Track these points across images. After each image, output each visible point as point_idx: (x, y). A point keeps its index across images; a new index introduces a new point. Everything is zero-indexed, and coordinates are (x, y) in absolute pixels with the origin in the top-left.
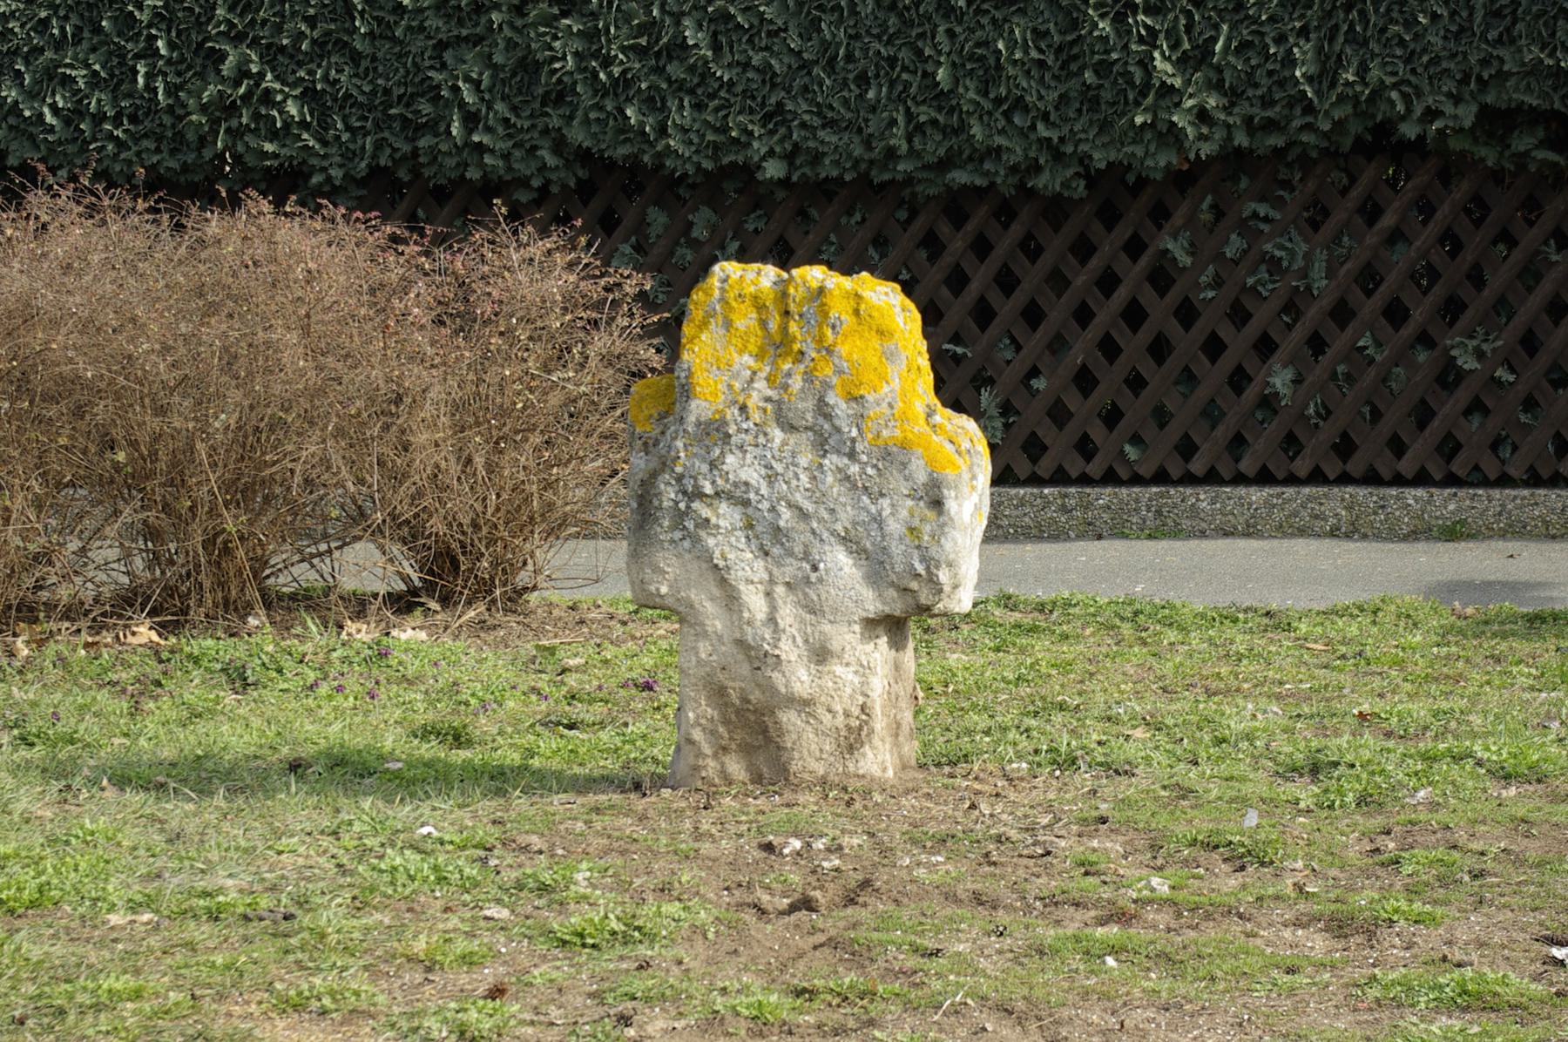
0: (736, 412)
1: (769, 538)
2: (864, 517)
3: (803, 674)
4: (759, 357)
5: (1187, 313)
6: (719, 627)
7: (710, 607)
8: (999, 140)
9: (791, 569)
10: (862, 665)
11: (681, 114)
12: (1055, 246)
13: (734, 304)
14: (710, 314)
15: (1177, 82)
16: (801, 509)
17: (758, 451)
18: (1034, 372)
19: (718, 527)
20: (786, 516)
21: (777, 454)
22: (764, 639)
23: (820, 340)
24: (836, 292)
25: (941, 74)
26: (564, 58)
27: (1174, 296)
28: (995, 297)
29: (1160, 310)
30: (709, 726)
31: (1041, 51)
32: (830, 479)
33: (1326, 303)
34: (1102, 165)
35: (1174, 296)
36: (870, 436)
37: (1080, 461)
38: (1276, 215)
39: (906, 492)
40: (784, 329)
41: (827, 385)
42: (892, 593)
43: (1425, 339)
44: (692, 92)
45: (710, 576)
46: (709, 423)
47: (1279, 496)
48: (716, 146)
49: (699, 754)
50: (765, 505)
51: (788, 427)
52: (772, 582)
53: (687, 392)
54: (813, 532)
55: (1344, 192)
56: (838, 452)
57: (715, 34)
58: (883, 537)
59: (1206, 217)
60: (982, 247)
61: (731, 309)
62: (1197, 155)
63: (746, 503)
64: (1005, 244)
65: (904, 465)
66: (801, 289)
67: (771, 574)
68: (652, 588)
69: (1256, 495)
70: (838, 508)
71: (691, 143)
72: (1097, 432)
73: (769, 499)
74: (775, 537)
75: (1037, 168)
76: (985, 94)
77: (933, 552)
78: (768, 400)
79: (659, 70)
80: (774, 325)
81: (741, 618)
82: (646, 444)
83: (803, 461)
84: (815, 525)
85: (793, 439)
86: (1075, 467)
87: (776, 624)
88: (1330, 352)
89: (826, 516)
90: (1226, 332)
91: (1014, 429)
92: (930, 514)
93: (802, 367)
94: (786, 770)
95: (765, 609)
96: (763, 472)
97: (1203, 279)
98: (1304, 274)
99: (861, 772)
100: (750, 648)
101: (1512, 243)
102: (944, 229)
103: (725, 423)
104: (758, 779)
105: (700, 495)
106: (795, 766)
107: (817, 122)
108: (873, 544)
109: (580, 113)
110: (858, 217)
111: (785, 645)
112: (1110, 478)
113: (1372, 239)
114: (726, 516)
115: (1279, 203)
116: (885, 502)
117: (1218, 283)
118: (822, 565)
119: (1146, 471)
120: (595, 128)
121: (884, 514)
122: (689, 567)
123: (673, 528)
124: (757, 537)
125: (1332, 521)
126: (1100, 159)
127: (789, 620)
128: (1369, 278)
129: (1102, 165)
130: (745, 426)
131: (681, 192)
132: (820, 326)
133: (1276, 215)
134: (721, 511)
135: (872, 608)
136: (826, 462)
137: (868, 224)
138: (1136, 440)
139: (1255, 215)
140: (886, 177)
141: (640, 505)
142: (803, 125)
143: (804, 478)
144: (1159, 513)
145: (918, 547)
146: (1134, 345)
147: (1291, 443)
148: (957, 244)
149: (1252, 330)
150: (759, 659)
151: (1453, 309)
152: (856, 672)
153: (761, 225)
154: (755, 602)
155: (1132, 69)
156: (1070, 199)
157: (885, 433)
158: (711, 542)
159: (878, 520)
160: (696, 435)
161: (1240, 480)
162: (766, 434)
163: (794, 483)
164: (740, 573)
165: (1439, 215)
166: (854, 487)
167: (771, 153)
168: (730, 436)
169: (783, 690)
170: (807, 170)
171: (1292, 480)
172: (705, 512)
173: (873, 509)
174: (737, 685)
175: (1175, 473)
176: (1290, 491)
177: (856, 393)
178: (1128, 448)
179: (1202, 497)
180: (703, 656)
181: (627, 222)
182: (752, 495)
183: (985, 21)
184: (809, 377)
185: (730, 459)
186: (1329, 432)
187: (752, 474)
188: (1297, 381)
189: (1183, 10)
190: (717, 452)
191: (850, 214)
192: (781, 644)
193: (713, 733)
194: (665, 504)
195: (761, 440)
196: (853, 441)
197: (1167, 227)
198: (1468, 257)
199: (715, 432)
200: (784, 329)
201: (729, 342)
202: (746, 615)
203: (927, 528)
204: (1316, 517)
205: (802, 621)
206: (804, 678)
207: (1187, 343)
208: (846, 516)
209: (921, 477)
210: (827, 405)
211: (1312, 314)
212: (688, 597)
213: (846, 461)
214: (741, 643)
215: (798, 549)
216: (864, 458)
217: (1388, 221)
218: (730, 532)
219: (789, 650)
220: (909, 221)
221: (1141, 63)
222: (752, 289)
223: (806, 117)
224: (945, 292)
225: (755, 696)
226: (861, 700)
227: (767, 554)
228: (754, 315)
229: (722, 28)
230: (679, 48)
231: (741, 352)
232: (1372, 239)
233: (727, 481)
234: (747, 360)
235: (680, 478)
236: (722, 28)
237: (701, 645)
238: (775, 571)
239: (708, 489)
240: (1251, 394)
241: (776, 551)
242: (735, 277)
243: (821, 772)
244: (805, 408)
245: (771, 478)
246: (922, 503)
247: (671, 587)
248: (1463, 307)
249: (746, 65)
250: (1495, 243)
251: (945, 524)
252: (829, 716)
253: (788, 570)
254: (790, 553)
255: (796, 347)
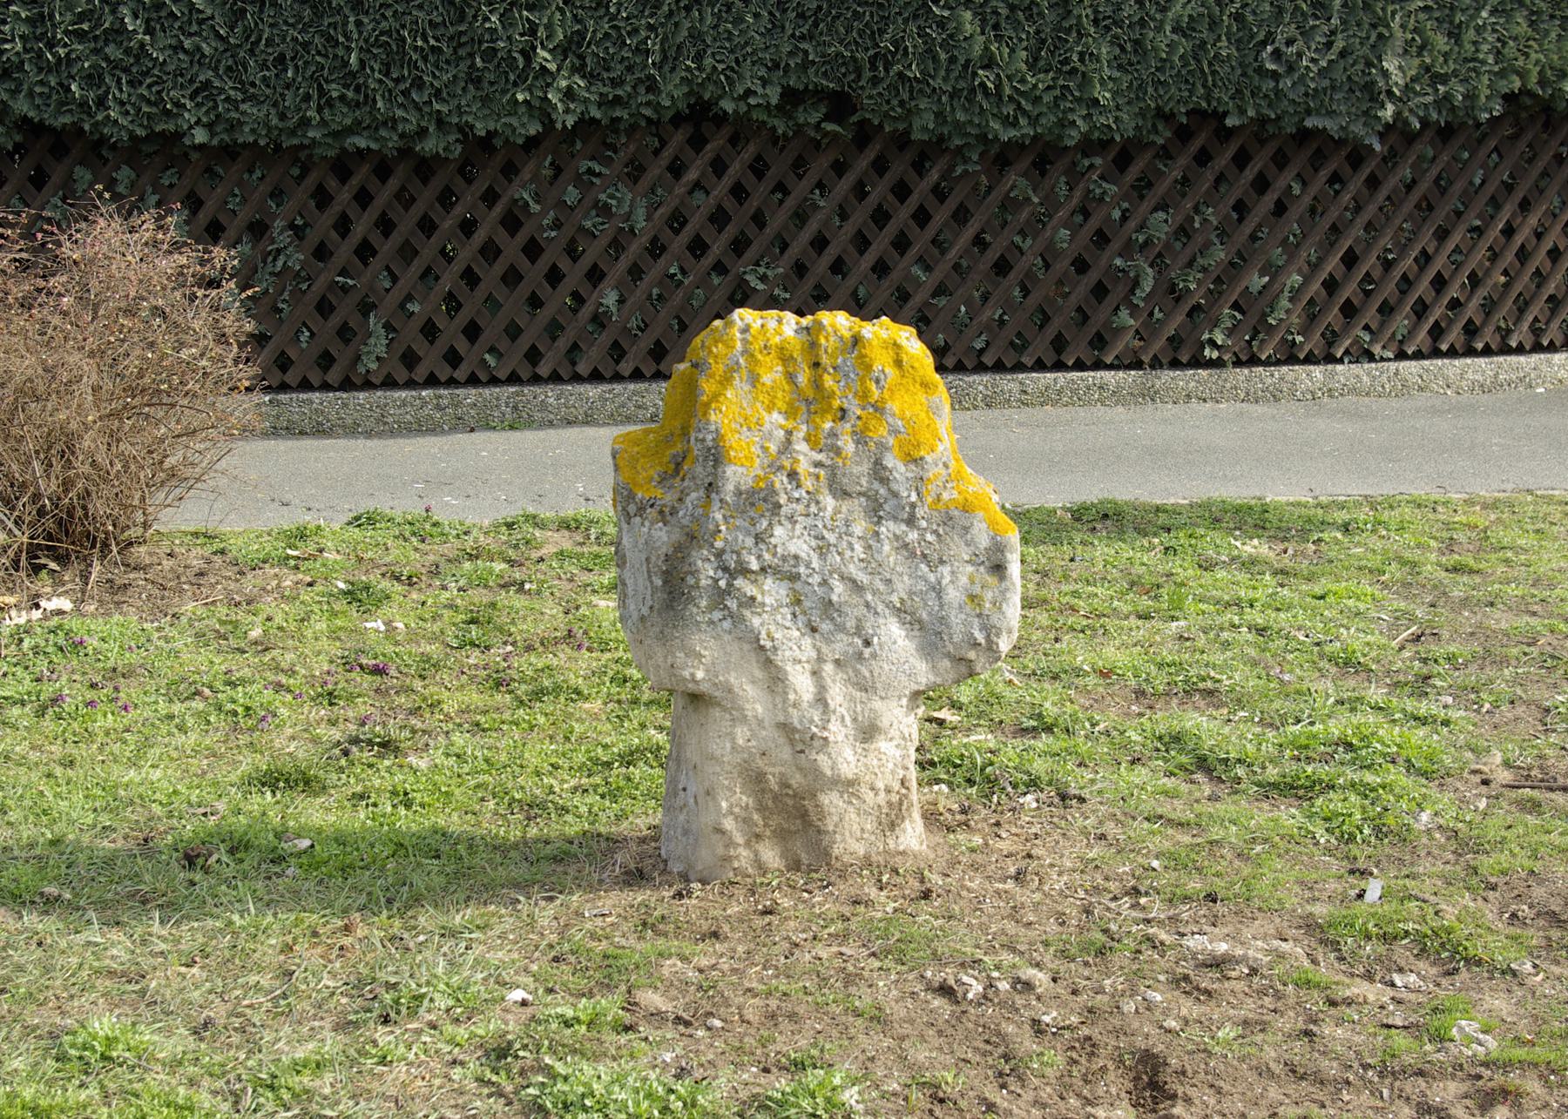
0: (785, 480)
1: (818, 614)
2: (921, 586)
3: (848, 753)
4: (790, 413)
5: (533, 250)
6: (760, 710)
7: (750, 691)
8: (399, 113)
9: (842, 645)
10: (904, 738)
11: (119, 91)
12: (426, 197)
13: (759, 357)
14: (733, 368)
15: (552, 67)
16: (854, 581)
17: (810, 521)
18: (409, 298)
19: (763, 604)
20: (839, 590)
21: (829, 523)
22: (812, 721)
23: (864, 395)
24: (875, 343)
25: (353, 59)
26: (13, 40)
27: (522, 237)
28: (375, 239)
29: (512, 249)
30: (743, 814)
31: (437, 40)
32: (887, 548)
33: (644, 240)
34: (483, 133)
35: (522, 237)
36: (930, 500)
37: (448, 369)
38: (605, 171)
39: (967, 558)
40: (817, 384)
41: (882, 447)
42: (946, 663)
43: (720, 268)
44: (126, 70)
45: (753, 657)
46: (752, 492)
47: (610, 392)
48: (149, 116)
49: (730, 843)
50: (816, 579)
51: (842, 494)
52: (820, 659)
53: (716, 456)
54: (867, 605)
55: (656, 152)
56: (895, 519)
57: (148, 21)
58: (941, 606)
59: (547, 172)
60: (363, 198)
61: (757, 362)
62: (564, 126)
63: (794, 578)
64: (384, 196)
65: (966, 529)
66: (832, 339)
67: (819, 651)
68: (686, 674)
69: (592, 391)
70: (895, 578)
71: (127, 113)
72: (462, 346)
73: (821, 573)
74: (825, 612)
75: (422, 133)
76: (387, 74)
77: (994, 620)
78: (818, 464)
79: (96, 51)
80: (803, 378)
81: (785, 701)
82: (661, 512)
83: (859, 528)
84: (869, 597)
85: (845, 506)
86: (444, 373)
87: (826, 705)
88: (647, 279)
89: (882, 587)
90: (564, 264)
91: (395, 345)
92: (991, 580)
93: (848, 426)
94: (828, 854)
95: (812, 689)
96: (814, 543)
97: (546, 222)
98: (628, 217)
99: (901, 848)
100: (794, 730)
101: (786, 193)
102: (332, 184)
103: (774, 492)
104: (795, 866)
105: (744, 571)
106: (836, 850)
107: (240, 96)
108: (930, 614)
109: (25, 87)
110: (258, 173)
111: (834, 726)
112: (473, 381)
113: (680, 190)
114: (772, 592)
115: (607, 162)
116: (945, 570)
117: (557, 225)
118: (875, 639)
119: (502, 375)
120: (38, 101)
121: (944, 582)
122: (728, 649)
123: (711, 608)
124: (804, 613)
125: (652, 410)
126: (480, 129)
127: (839, 699)
128: (677, 221)
129: (483, 133)
130: (797, 495)
131: (104, 153)
132: (863, 383)
133: (605, 171)
134: (766, 588)
135: (924, 681)
136: (883, 529)
137: (268, 179)
138: (492, 350)
139: (590, 171)
140: (295, 141)
141: (665, 582)
142: (228, 99)
143: (858, 548)
144: (515, 408)
145: (979, 616)
146: (491, 276)
147: (617, 352)
148: (344, 197)
149: (585, 263)
150: (801, 741)
151: (739, 246)
152: (897, 746)
153: (174, 180)
154: (801, 683)
155: (515, 55)
156: (447, 159)
157: (945, 496)
158: (756, 621)
159: (938, 590)
160: (736, 505)
161: (577, 378)
162: (818, 503)
163: (848, 553)
164: (787, 653)
165: (731, 171)
166: (913, 554)
167: (198, 122)
168: (780, 506)
169: (829, 773)
170: (226, 137)
171: (618, 378)
172: (750, 589)
173: (932, 578)
174: (777, 770)
175: (525, 375)
176: (618, 387)
177: (916, 455)
178: (487, 356)
179: (549, 394)
180: (741, 742)
181: (56, 178)
182: (802, 570)
183: (389, 13)
184: (860, 438)
185: (779, 531)
186: (646, 342)
187: (801, 546)
188: (621, 301)
189: (558, 8)
190: (765, 524)
191: (251, 172)
192: (830, 726)
193: (747, 821)
194: (703, 582)
195: (813, 509)
196: (913, 506)
197: (517, 181)
198: (753, 203)
199: (760, 502)
200: (817, 384)
201: (756, 399)
202: (792, 697)
203: (989, 595)
204: (639, 407)
205: (852, 700)
206: (851, 758)
207: (534, 274)
208: (902, 585)
209: (984, 542)
210: (885, 468)
211: (635, 249)
212: (727, 681)
213: (904, 527)
214: (786, 728)
215: (851, 624)
216: (924, 524)
217: (692, 175)
218: (775, 610)
219: (838, 732)
220: (301, 177)
221: (522, 52)
222: (777, 339)
223: (232, 93)
224: (334, 235)
225: (796, 780)
226: (901, 773)
227: (814, 630)
228: (780, 368)
229: (154, 15)
230: (119, 31)
231: (769, 409)
232: (680, 190)
233: (774, 555)
234: (776, 417)
235: (719, 554)
236: (154, 15)
237: (738, 730)
238: (825, 649)
239: (755, 566)
240: (586, 312)
241: (825, 626)
242: (756, 325)
243: (862, 852)
244: (858, 472)
245: (823, 550)
246: (982, 569)
247: (707, 671)
248: (749, 243)
249: (179, 47)
250: (773, 192)
251: (1007, 589)
252: (871, 794)
253: (838, 646)
254: (841, 628)
255: (836, 403)
